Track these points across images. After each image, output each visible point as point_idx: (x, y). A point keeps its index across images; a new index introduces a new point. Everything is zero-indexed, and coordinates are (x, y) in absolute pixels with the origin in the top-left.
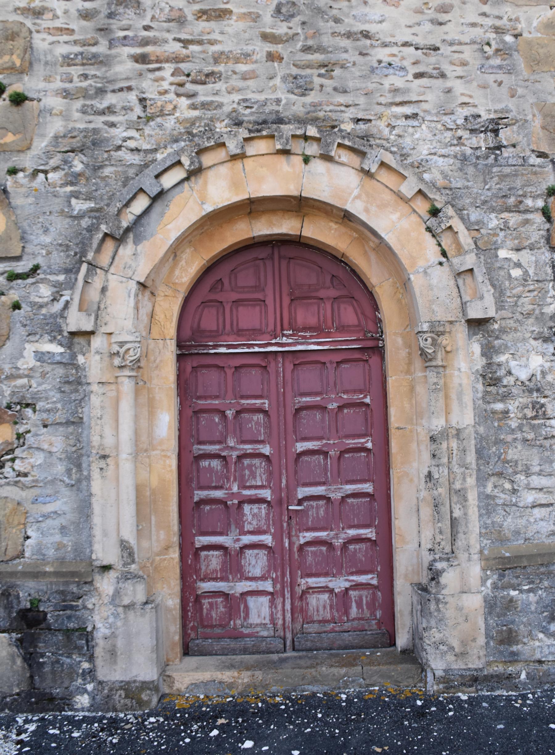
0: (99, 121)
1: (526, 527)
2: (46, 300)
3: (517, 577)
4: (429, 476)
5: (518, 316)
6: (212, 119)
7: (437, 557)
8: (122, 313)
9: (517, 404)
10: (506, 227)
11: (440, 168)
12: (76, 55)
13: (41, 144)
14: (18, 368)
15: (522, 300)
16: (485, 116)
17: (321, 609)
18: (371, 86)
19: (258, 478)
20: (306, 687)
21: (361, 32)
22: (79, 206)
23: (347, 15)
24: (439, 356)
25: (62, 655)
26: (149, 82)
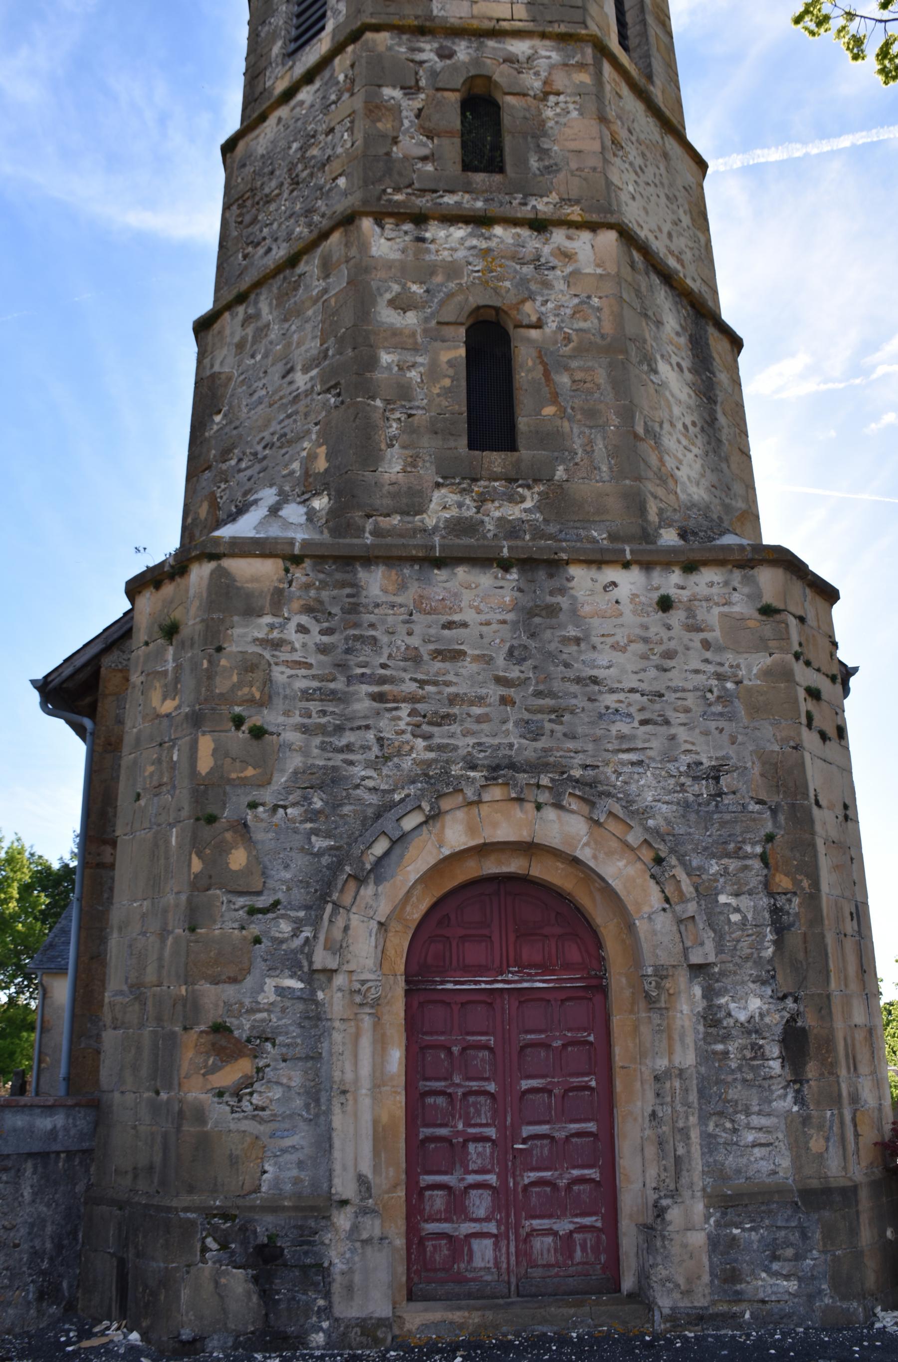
0: (338, 759)
1: (747, 1166)
2: (286, 935)
3: (739, 1215)
4: (654, 1114)
5: (737, 960)
6: (447, 762)
7: (662, 1194)
8: (363, 949)
9: (736, 1045)
10: (726, 872)
11: (664, 813)
12: (315, 690)
13: (281, 780)
14: (258, 1003)
15: (741, 944)
16: (707, 763)
17: (545, 1252)
18: (599, 732)
19: (483, 1116)
20: (536, 1327)
21: (590, 677)
22: (319, 843)
23: (577, 661)
24: (663, 999)
25: (297, 1292)
26: (386, 722)
